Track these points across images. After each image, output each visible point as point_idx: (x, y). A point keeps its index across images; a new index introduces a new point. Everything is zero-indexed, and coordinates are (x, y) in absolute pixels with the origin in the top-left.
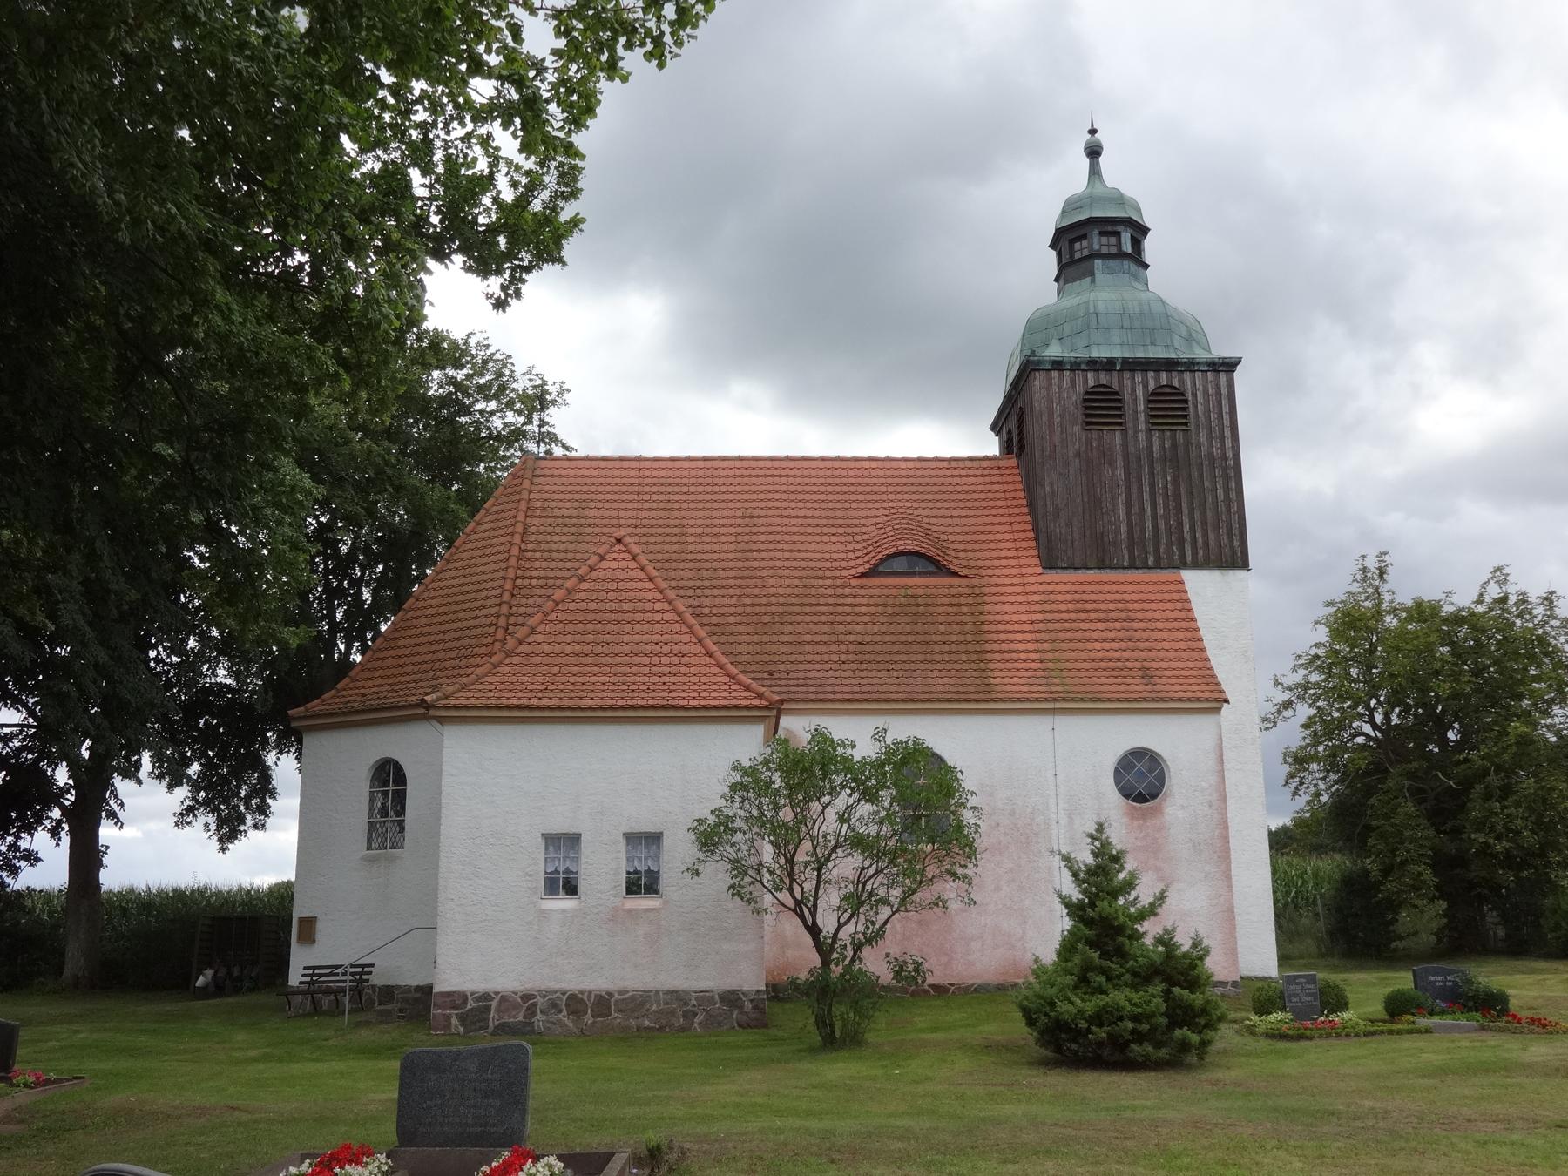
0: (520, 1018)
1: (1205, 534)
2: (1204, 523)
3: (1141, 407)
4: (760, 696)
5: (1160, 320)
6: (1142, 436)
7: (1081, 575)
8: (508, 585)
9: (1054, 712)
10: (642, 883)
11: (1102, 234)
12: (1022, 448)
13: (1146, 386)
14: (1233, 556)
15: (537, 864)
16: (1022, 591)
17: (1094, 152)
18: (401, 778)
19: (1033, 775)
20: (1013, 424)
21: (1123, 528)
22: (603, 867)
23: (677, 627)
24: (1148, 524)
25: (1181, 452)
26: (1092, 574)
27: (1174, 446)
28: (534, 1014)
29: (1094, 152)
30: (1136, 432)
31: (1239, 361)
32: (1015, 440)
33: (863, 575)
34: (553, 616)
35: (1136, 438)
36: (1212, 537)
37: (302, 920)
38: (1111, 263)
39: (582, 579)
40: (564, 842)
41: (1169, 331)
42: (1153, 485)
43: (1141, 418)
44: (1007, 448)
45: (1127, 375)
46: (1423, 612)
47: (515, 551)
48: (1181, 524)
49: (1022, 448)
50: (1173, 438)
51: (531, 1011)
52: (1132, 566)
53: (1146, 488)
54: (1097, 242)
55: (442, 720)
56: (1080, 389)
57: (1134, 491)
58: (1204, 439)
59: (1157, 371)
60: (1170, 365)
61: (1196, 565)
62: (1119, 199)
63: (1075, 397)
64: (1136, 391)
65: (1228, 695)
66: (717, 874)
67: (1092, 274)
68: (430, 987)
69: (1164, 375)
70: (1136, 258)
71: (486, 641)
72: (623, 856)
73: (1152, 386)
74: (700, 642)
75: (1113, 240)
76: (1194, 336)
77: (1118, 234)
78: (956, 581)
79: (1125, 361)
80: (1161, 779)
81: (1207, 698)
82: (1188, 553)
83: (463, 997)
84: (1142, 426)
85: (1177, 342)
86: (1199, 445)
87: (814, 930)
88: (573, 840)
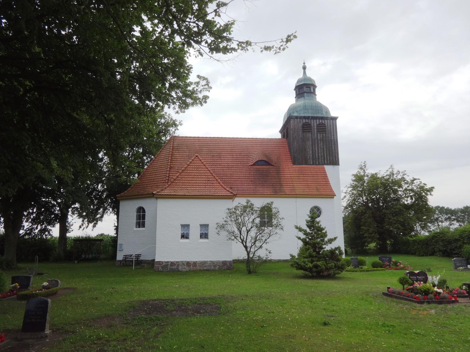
0: (176, 267)
1: (330, 157)
2: (329, 155)
3: (315, 128)
4: (232, 193)
5: (320, 107)
6: (316, 134)
7: (301, 166)
8: (169, 166)
9: (296, 197)
10: (204, 236)
11: (306, 87)
12: (287, 136)
13: (317, 123)
14: (335, 161)
15: (179, 232)
16: (290, 170)
17: (304, 68)
18: (144, 211)
19: (292, 213)
20: (286, 130)
21: (311, 155)
22: (195, 232)
23: (211, 177)
24: (317, 154)
25: (324, 138)
26: (304, 166)
27: (323, 137)
28: (179, 266)
29: (304, 68)
30: (314, 133)
31: (337, 118)
32: (286, 135)
33: (251, 165)
34: (182, 174)
35: (314, 135)
36: (331, 158)
37: (120, 244)
38: (309, 94)
39: (188, 165)
40: (185, 227)
41: (322, 110)
42: (318, 145)
43: (316, 130)
44: (283, 136)
45: (312, 120)
46: (374, 177)
47: (170, 158)
48: (324, 155)
49: (287, 136)
50: (323, 135)
51: (178, 265)
52: (313, 164)
53: (316, 146)
54: (305, 89)
55: (157, 198)
56: (302, 123)
57: (314, 147)
58: (329, 135)
59: (319, 120)
60: (322, 118)
61: (327, 164)
62: (310, 79)
63: (300, 125)
64: (314, 123)
65: (336, 194)
66: (224, 234)
67: (304, 97)
68: (154, 260)
69: (321, 120)
70: (314, 93)
71: (164, 179)
72: (199, 229)
73: (318, 123)
74: (217, 180)
75: (309, 89)
76: (327, 112)
77: (310, 88)
78: (272, 167)
79: (312, 117)
80: (320, 213)
81: (331, 195)
82: (326, 161)
83: (162, 262)
84: (316, 132)
85: (324, 113)
86: (328, 137)
87: (246, 247)
88: (188, 226)
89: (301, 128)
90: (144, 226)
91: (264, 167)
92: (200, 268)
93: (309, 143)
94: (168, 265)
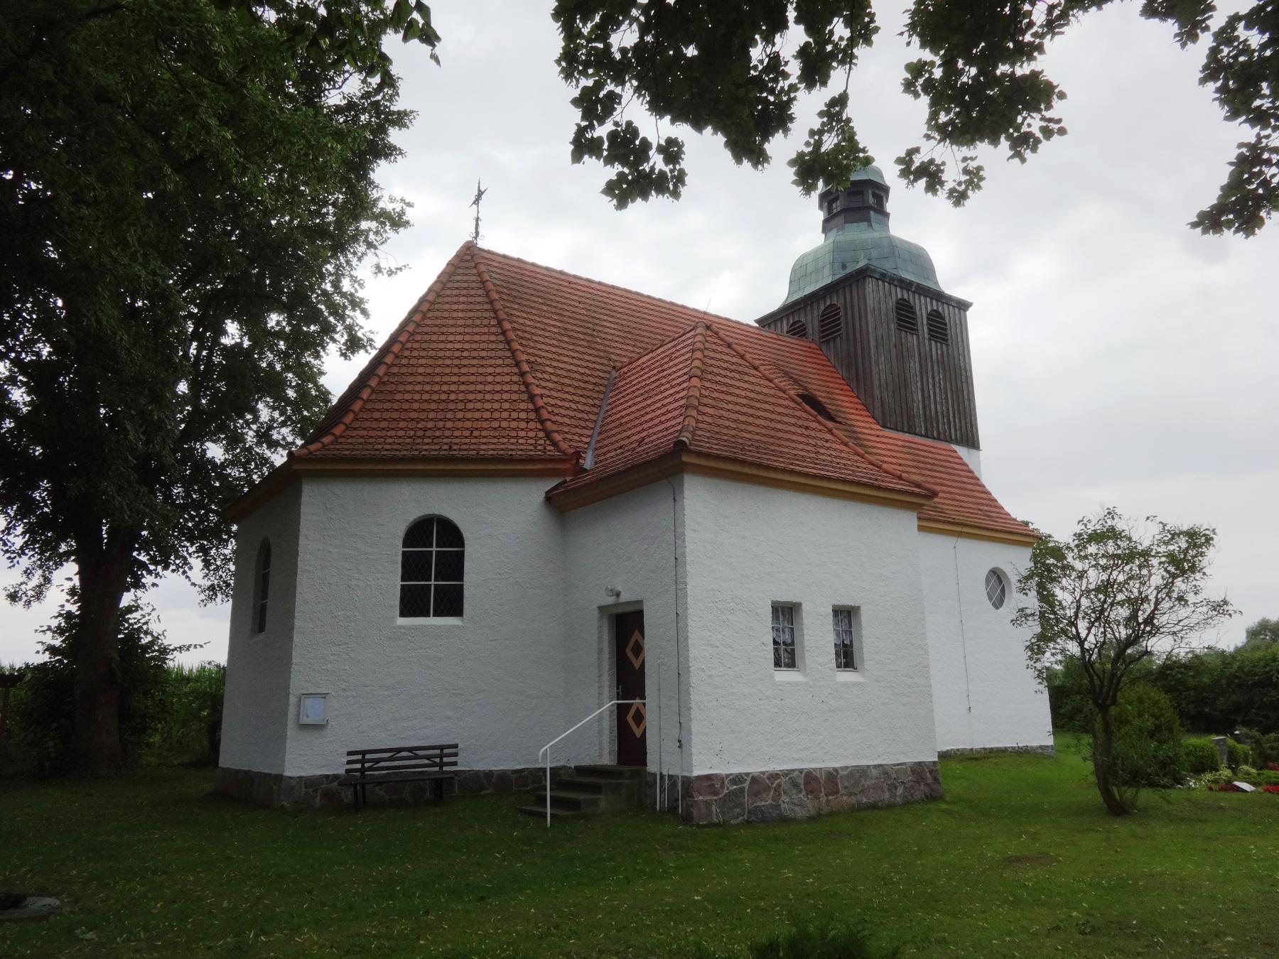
52: (926, 436)
63: (891, 303)
89: (893, 315)
90: (451, 604)
91: (302, 467)
92: (854, 800)
93: (914, 365)
94: (742, 790)
